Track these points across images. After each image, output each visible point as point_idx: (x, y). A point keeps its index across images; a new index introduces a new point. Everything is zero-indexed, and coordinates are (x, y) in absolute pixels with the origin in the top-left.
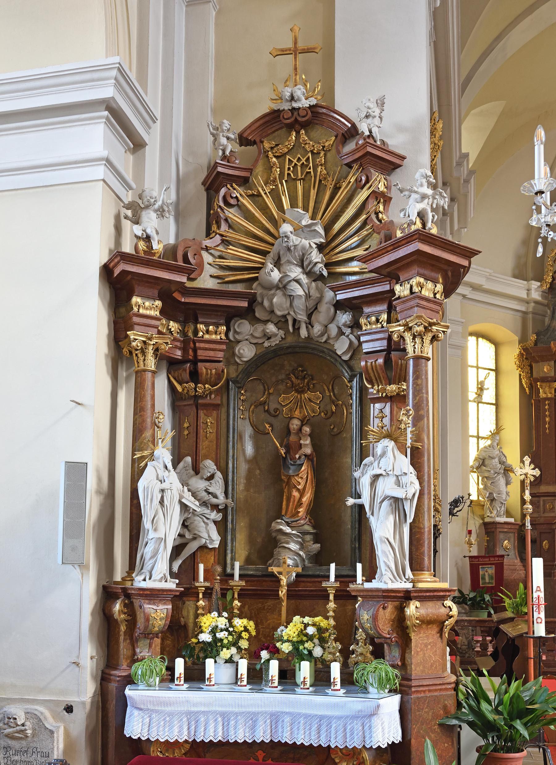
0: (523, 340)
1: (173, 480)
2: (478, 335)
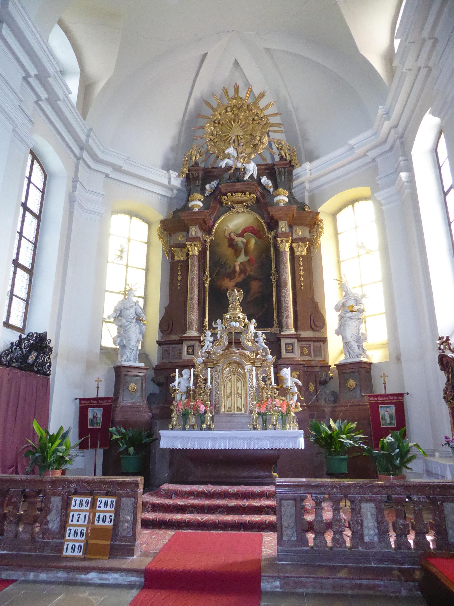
2: (132, 214)
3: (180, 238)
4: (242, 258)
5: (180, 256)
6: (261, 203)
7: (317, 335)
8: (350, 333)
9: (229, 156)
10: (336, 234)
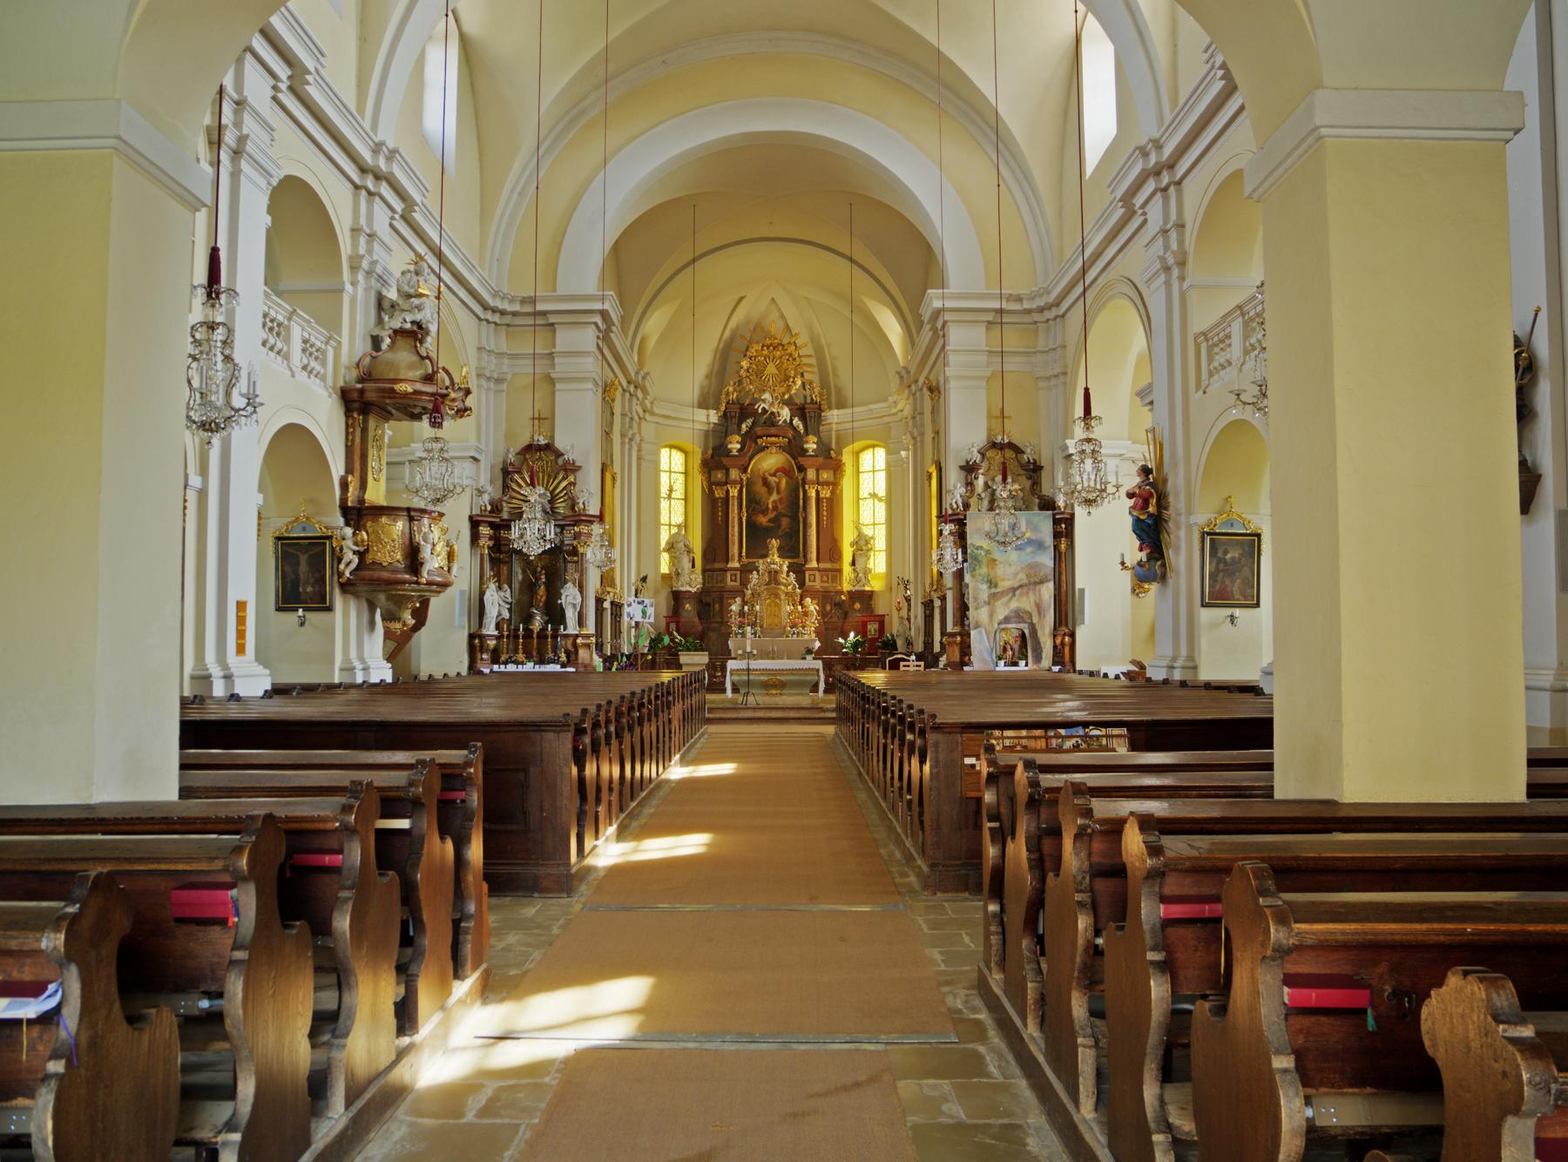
0: (704, 453)
2: (671, 447)
3: (720, 475)
4: (775, 497)
5: (719, 493)
6: (795, 449)
7: (836, 566)
8: (859, 566)
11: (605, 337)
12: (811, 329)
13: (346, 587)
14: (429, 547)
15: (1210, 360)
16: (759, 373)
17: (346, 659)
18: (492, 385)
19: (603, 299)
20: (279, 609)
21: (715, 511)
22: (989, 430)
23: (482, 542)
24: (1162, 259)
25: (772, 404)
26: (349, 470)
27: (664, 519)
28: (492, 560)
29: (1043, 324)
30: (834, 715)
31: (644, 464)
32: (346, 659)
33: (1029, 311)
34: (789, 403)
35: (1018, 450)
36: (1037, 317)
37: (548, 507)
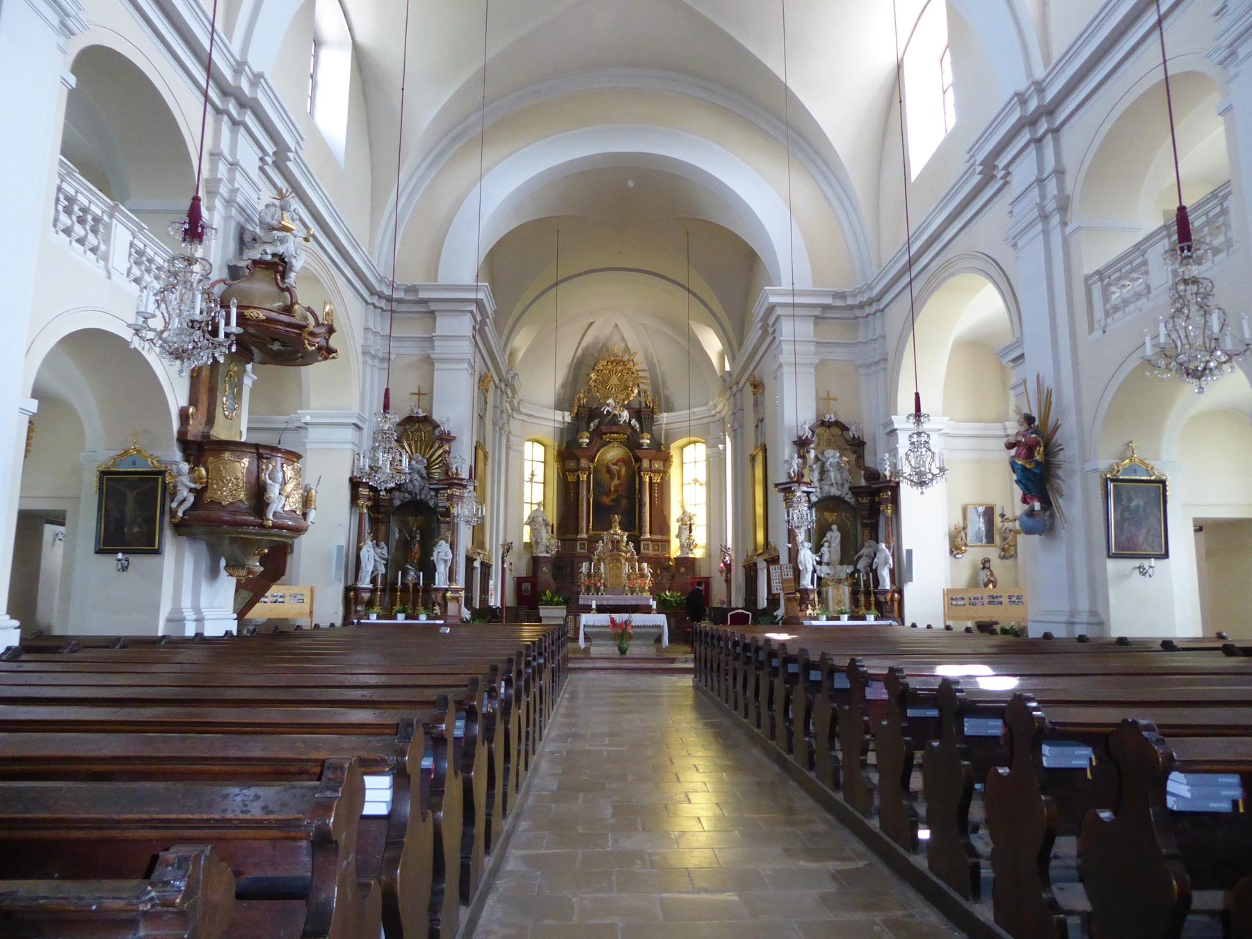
1: (372, 551)
2: (534, 441)
3: (572, 464)
4: (616, 482)
5: (571, 478)
6: (632, 443)
7: (664, 538)
9: (608, 405)
10: (682, 463)
11: (479, 329)
12: (645, 350)
13: (181, 528)
14: (277, 488)
15: (1106, 299)
16: (604, 383)
17: (177, 609)
18: (377, 363)
19: (477, 289)
20: (99, 551)
21: (568, 493)
22: (818, 410)
23: (361, 502)
24: (1041, 207)
25: (614, 408)
26: (193, 400)
27: (527, 498)
28: (371, 520)
29: (866, 319)
30: (692, 665)
31: (512, 453)
32: (177, 609)
33: (851, 307)
34: (628, 407)
35: (844, 428)
36: (858, 313)
37: (424, 472)
